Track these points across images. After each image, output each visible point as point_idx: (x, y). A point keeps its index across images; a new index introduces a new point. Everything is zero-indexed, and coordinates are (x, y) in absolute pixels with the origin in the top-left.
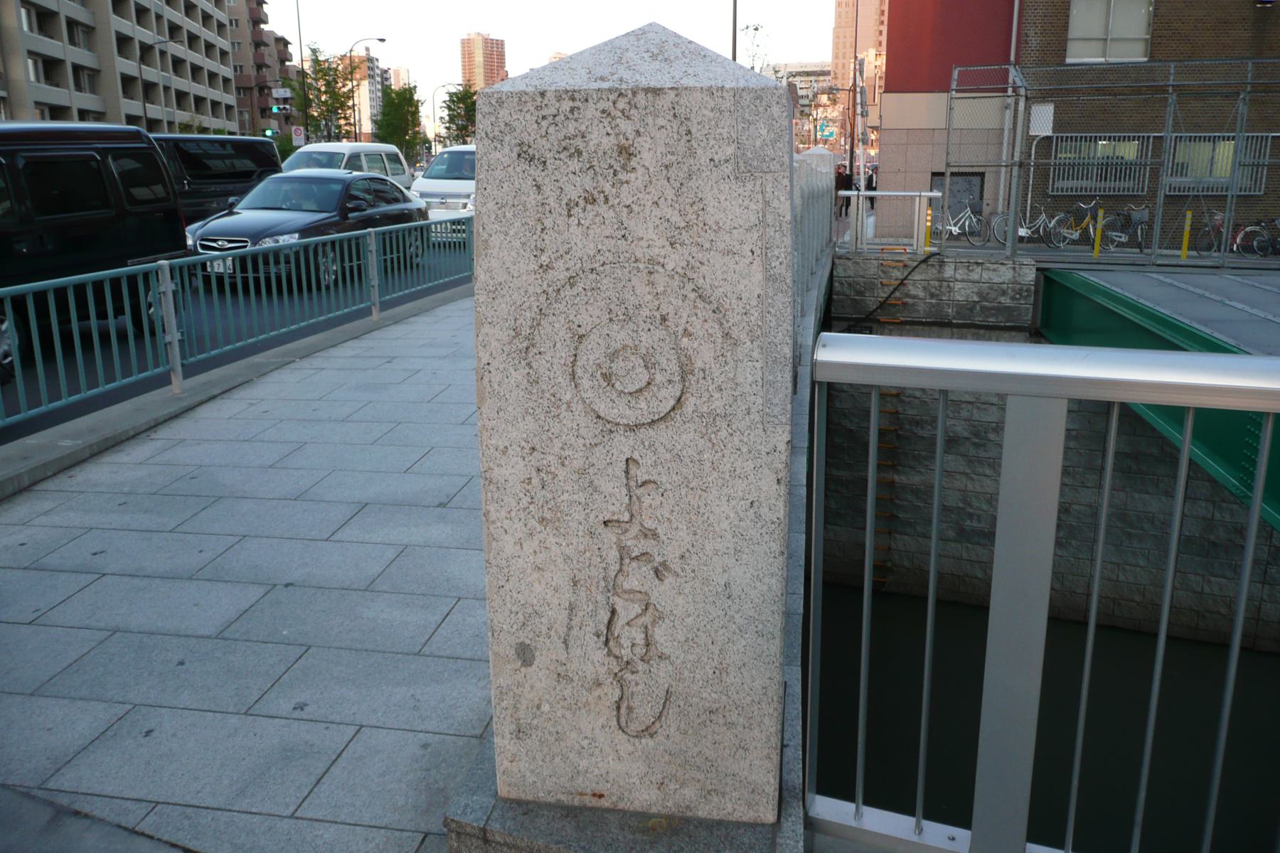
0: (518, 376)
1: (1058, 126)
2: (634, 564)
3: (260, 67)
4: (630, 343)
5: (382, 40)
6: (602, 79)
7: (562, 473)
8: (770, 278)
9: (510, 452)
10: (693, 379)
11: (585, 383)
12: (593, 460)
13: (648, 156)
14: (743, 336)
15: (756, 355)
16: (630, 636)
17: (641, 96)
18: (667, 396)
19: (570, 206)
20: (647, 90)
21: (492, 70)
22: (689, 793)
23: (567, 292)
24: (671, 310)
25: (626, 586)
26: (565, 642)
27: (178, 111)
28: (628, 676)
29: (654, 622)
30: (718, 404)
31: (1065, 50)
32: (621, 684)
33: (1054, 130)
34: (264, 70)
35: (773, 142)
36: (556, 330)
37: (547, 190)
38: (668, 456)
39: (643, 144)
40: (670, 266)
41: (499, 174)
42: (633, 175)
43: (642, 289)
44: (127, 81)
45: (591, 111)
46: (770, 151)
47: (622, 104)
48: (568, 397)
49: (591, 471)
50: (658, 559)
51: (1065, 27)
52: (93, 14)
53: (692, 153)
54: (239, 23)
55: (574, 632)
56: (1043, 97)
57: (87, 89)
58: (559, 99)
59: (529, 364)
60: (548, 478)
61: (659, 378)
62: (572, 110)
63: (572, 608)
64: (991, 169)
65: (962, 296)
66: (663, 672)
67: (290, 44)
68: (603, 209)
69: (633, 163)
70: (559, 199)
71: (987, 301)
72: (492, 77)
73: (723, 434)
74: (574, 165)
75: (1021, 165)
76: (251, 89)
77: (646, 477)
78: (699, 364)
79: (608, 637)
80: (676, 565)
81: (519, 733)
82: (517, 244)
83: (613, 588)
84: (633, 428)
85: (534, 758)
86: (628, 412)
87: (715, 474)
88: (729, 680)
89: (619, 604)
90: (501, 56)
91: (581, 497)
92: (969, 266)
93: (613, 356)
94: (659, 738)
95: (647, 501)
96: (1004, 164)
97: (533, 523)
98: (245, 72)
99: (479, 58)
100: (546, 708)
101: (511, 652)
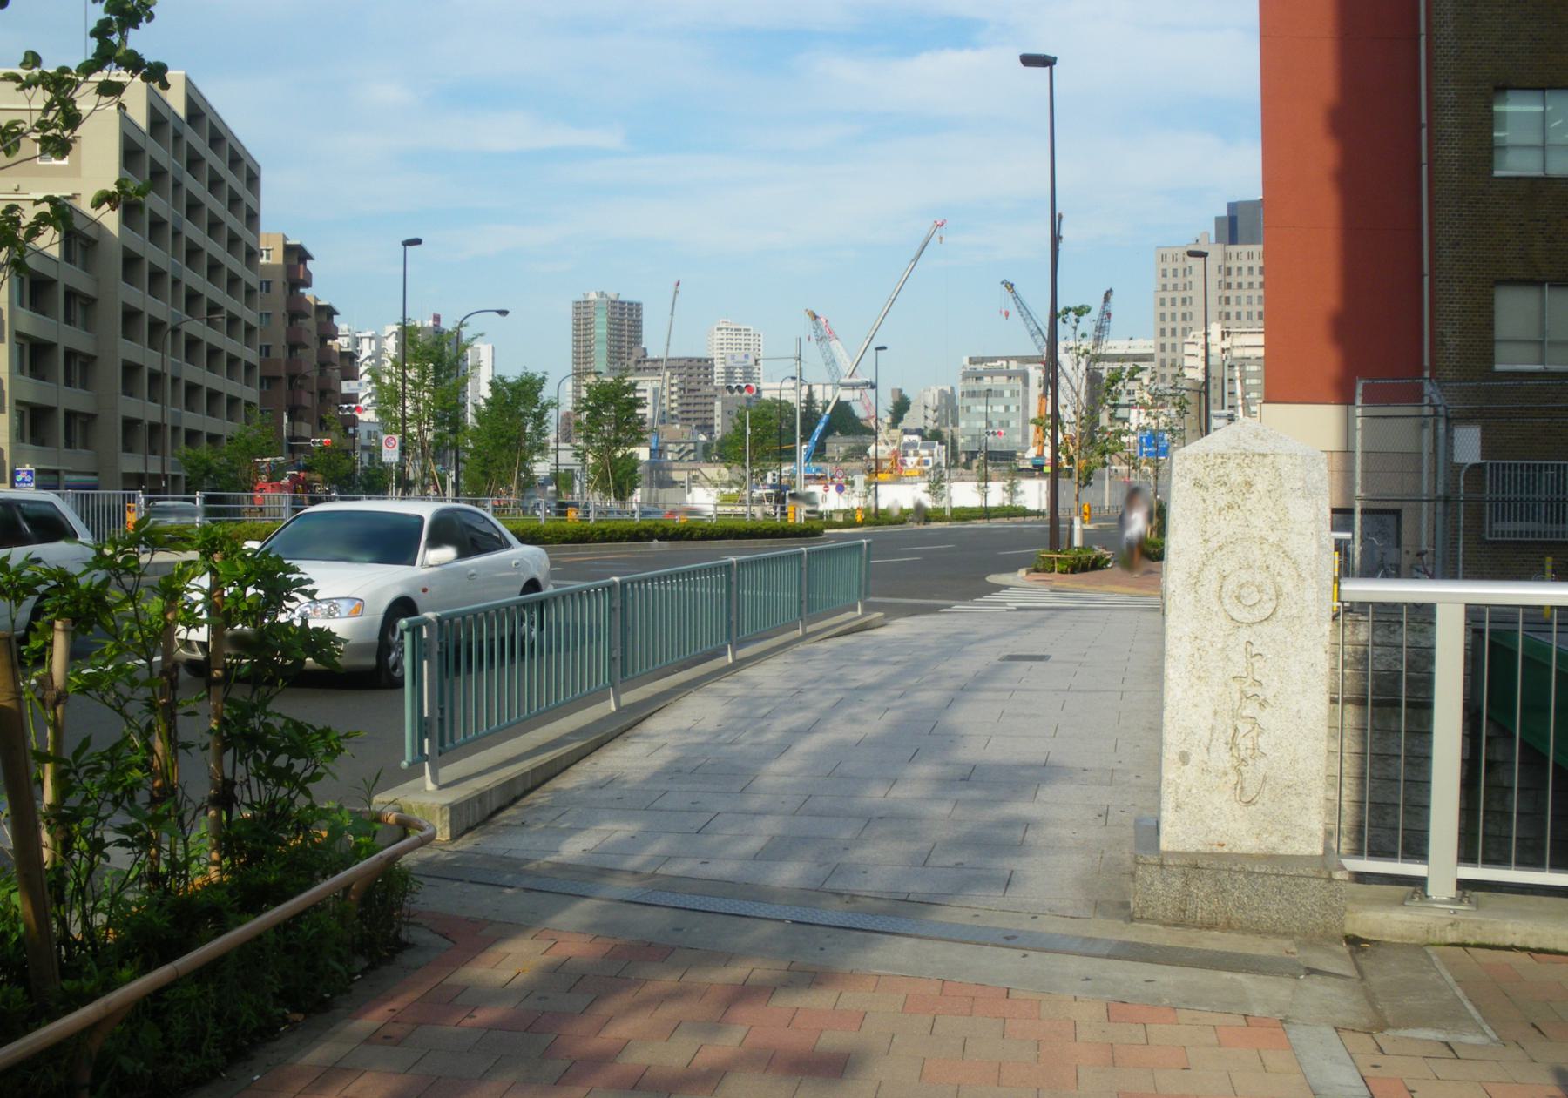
0: (1190, 598)
1: (1488, 448)
2: (1248, 701)
3: (293, 347)
4: (1250, 579)
5: (503, 313)
6: (1234, 448)
7: (1211, 650)
8: (1321, 547)
9: (1184, 639)
10: (1282, 598)
11: (1226, 601)
12: (1228, 643)
13: (1260, 486)
14: (1308, 577)
15: (1314, 585)
16: (1244, 743)
17: (1256, 457)
18: (1269, 607)
19: (1220, 510)
20: (1260, 455)
21: (620, 347)
22: (1274, 839)
23: (1218, 554)
24: (1271, 562)
25: (1244, 714)
26: (1208, 749)
27: (186, 412)
28: (1243, 768)
29: (1258, 735)
30: (1295, 611)
31: (1493, 354)
32: (1240, 772)
33: (1483, 456)
34: (299, 351)
35: (1322, 480)
36: (1211, 575)
37: (1208, 502)
38: (1268, 640)
39: (1258, 479)
40: (1271, 540)
41: (1184, 493)
42: (1252, 496)
43: (1257, 553)
44: (130, 370)
45: (1231, 464)
46: (1319, 485)
47: (1247, 461)
48: (1216, 609)
49: (1227, 649)
50: (1262, 698)
51: (1490, 325)
52: (97, 280)
53: (1281, 485)
54: (272, 286)
55: (1214, 743)
56: (1467, 418)
57: (78, 385)
58: (1216, 457)
59: (1196, 592)
60: (1203, 654)
61: (1265, 598)
62: (1222, 463)
63: (1213, 728)
64: (1411, 504)
65: (1382, 664)
66: (1262, 764)
67: (337, 314)
68: (1237, 512)
69: (1252, 489)
70: (1215, 506)
71: (1415, 671)
72: (620, 359)
73: (1297, 627)
74: (1223, 489)
75: (1446, 500)
76: (278, 378)
77: (1256, 652)
78: (1285, 590)
79: (1232, 744)
80: (1271, 701)
81: (1178, 808)
82: (1192, 528)
83: (1235, 715)
84: (1250, 625)
85: (1185, 823)
86: (1249, 617)
87: (1293, 649)
88: (1298, 767)
89: (1240, 725)
90: (636, 325)
91: (1221, 664)
92: (1389, 626)
93: (1241, 587)
94: (1259, 806)
95: (1256, 665)
96: (1425, 498)
97: (1194, 679)
98: (273, 354)
99: (601, 329)
100: (1194, 791)
101: (1176, 757)
